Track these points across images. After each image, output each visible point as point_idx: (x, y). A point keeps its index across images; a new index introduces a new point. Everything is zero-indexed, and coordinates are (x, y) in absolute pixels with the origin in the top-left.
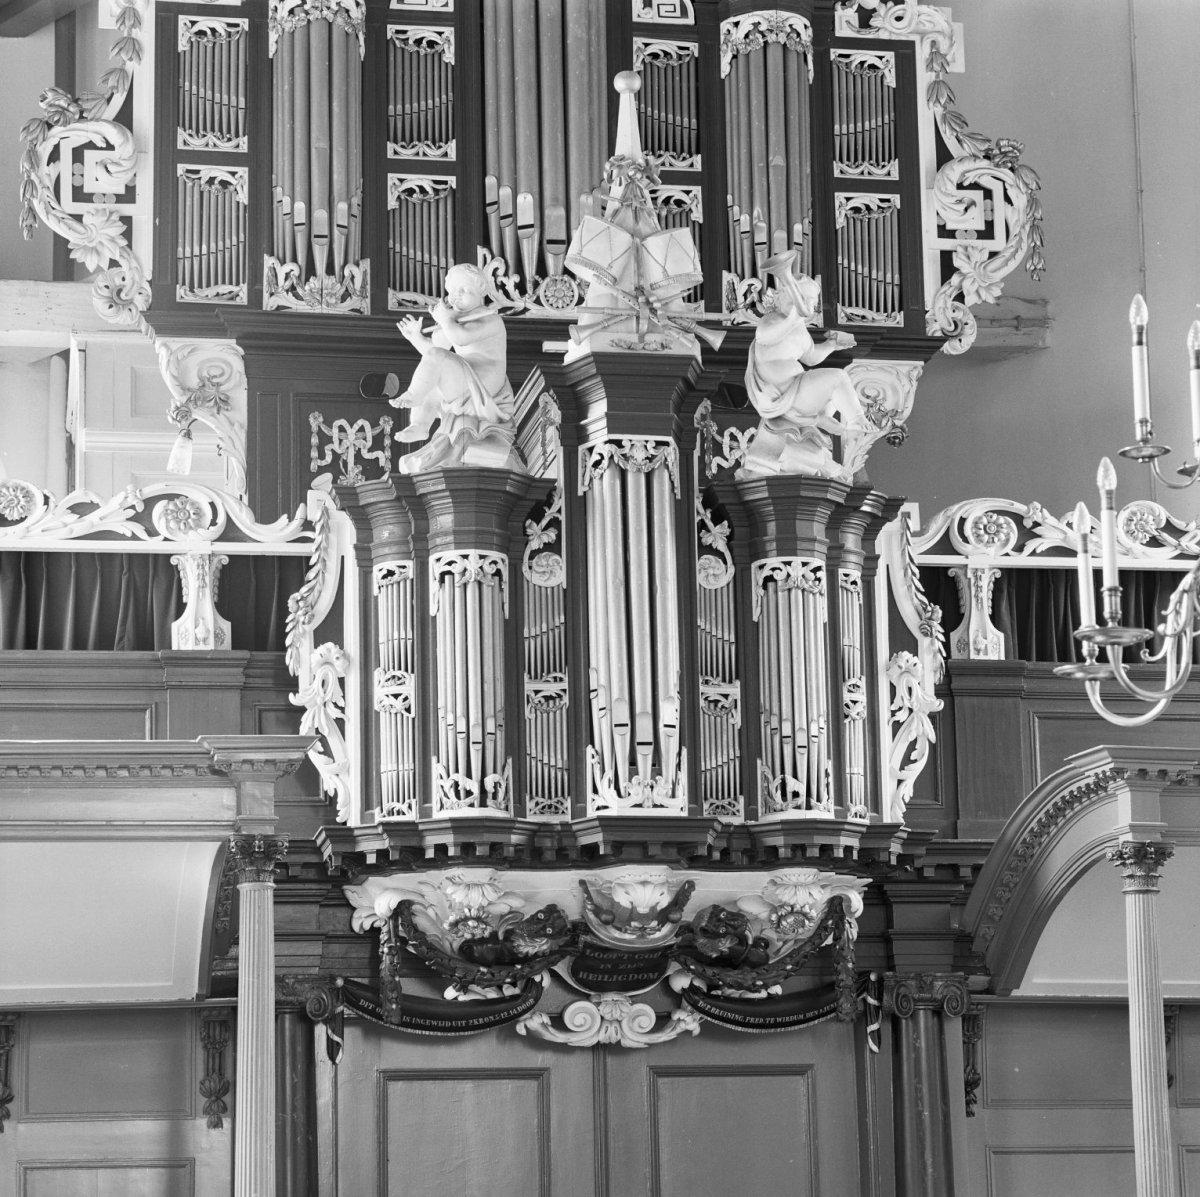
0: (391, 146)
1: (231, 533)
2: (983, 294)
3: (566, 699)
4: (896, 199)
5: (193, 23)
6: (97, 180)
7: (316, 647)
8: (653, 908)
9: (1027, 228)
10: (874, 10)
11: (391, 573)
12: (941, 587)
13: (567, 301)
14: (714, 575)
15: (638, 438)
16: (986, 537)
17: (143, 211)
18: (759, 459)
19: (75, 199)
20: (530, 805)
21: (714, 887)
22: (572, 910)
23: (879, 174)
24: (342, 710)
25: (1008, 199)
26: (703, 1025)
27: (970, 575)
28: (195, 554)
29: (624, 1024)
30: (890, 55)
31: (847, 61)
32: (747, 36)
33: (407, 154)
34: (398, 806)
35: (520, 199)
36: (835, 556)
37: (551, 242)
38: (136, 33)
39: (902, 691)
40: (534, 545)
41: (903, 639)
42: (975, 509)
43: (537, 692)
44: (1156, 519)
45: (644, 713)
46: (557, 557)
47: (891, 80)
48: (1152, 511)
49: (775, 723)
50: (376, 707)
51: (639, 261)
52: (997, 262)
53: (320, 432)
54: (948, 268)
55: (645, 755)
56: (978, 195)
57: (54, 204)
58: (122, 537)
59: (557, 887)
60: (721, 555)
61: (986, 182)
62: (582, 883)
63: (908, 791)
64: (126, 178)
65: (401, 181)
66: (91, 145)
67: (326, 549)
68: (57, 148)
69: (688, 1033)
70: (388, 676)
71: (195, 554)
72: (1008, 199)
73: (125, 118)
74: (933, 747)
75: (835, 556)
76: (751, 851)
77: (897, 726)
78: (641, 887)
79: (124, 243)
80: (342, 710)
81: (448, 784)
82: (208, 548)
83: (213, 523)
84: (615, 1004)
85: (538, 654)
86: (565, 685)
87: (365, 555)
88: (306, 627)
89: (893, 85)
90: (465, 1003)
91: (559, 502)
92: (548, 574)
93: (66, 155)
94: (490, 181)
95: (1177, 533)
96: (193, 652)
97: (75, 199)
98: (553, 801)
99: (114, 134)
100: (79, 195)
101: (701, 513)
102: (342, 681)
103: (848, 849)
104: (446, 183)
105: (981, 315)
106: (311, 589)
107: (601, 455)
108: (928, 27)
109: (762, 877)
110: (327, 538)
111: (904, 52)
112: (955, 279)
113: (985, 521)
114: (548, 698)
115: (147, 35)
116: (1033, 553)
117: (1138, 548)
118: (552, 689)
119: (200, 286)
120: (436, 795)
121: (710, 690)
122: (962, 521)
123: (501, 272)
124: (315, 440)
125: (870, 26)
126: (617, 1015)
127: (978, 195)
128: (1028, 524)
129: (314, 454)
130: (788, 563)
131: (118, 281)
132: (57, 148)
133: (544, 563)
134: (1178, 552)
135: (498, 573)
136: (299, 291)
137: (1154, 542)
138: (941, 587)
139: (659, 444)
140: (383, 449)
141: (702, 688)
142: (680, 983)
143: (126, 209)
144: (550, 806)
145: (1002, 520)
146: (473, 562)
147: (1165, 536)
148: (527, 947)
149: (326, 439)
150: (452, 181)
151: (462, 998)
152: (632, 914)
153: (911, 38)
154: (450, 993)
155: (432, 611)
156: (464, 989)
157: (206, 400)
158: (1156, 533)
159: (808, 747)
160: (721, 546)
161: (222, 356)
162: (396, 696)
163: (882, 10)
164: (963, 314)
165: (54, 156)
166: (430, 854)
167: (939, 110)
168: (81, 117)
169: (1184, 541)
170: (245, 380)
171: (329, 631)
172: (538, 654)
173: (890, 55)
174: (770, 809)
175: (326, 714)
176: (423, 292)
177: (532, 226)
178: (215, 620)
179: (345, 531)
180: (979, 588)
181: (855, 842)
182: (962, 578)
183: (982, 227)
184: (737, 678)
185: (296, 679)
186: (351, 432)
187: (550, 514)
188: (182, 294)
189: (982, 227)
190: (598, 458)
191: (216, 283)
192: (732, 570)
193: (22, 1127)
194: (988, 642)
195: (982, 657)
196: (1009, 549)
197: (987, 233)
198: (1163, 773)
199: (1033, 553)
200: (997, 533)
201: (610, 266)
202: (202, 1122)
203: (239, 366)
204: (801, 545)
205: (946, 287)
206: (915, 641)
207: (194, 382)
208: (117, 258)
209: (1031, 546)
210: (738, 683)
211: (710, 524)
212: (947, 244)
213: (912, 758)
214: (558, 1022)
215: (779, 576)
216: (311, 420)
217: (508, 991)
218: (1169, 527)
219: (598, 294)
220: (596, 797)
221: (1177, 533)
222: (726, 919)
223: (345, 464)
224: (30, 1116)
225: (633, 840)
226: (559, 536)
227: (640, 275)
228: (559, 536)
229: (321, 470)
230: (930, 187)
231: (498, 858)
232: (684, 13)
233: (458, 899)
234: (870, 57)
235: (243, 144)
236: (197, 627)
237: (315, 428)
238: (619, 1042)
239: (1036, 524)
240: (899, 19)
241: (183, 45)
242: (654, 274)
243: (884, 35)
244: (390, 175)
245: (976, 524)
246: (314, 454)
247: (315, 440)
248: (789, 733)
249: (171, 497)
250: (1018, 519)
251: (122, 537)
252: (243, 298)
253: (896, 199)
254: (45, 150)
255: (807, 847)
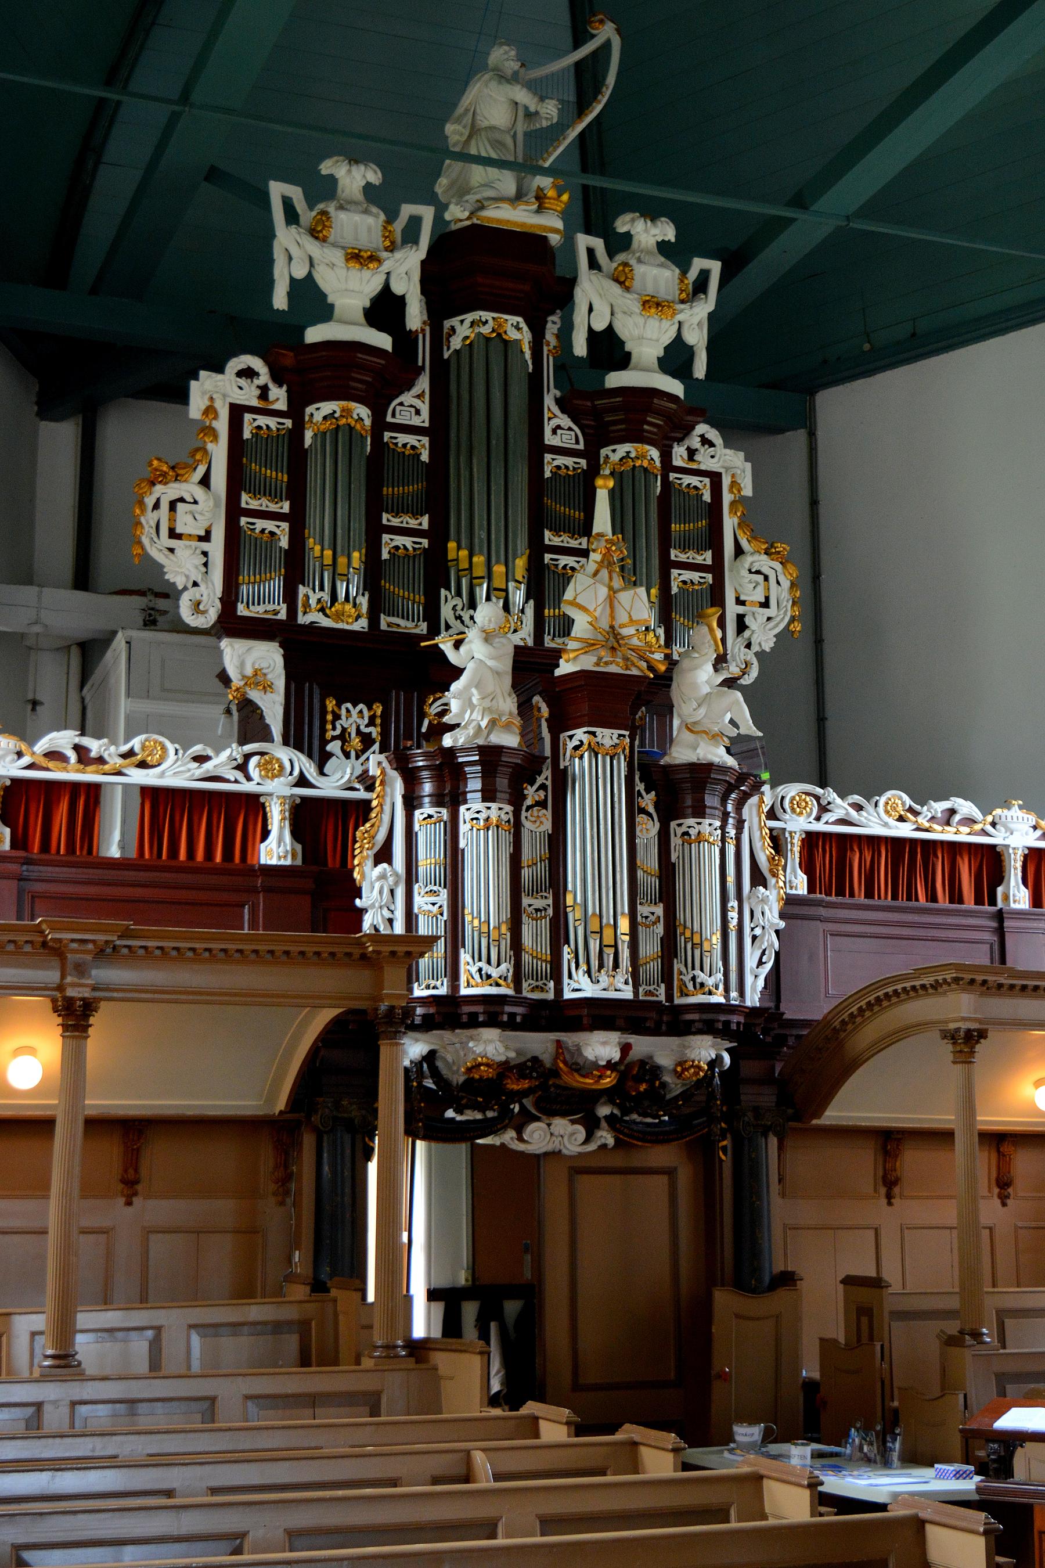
0: (385, 516)
1: (302, 781)
2: (763, 644)
3: (550, 911)
4: (709, 577)
5: (254, 420)
6: (185, 523)
7: (376, 865)
8: (609, 1062)
9: (791, 602)
10: (697, 450)
11: (430, 816)
12: (777, 841)
13: (506, 630)
14: (648, 830)
15: (607, 732)
16: (798, 810)
17: (217, 548)
18: (684, 751)
19: (170, 537)
20: (525, 985)
21: (643, 1045)
22: (547, 1059)
23: (699, 559)
24: (392, 912)
25: (778, 583)
26: (617, 1140)
27: (787, 835)
28: (277, 794)
29: (566, 1138)
30: (707, 481)
31: (679, 482)
32: (621, 460)
33: (395, 522)
34: (433, 983)
35: (475, 559)
36: (725, 816)
37: (496, 589)
38: (215, 424)
39: (758, 914)
40: (529, 802)
41: (758, 879)
42: (792, 790)
43: (530, 906)
44: (904, 804)
45: (608, 924)
46: (544, 811)
47: (707, 497)
48: (900, 798)
49: (688, 934)
50: (416, 910)
51: (612, 607)
52: (772, 624)
53: (333, 712)
54: (741, 626)
55: (610, 961)
56: (760, 578)
57: (156, 539)
58: (228, 781)
59: (539, 1043)
60: (650, 815)
61: (765, 570)
62: (558, 1042)
63: (761, 983)
64: (206, 525)
65: (392, 540)
66: (182, 500)
67: (383, 797)
68: (158, 500)
69: (604, 1146)
70: (428, 889)
71: (277, 794)
72: (778, 583)
73: (205, 482)
74: (777, 954)
75: (725, 816)
76: (676, 1021)
77: (754, 938)
78: (601, 1047)
79: (204, 569)
80: (392, 912)
81: (474, 970)
82: (289, 791)
83: (291, 774)
84: (561, 1125)
85: (539, 877)
86: (550, 901)
87: (411, 803)
88: (370, 852)
89: (709, 501)
90: (461, 1122)
91: (547, 773)
92: (538, 824)
93: (165, 506)
94: (452, 545)
95: (916, 813)
96: (276, 866)
97: (170, 537)
98: (540, 983)
99: (199, 493)
100: (173, 534)
101: (640, 787)
102: (392, 891)
103: (738, 1023)
104: (420, 543)
105: (760, 655)
106: (372, 826)
107: (581, 741)
108: (732, 465)
109: (673, 1041)
110: (383, 790)
111: (715, 478)
112: (747, 634)
113: (797, 798)
114: (537, 910)
115: (222, 426)
116: (827, 823)
117: (891, 822)
118: (539, 903)
119: (253, 604)
120: (463, 978)
121: (643, 910)
122: (783, 798)
123: (459, 608)
124: (330, 717)
125: (694, 461)
126: (562, 1133)
127: (760, 578)
128: (824, 802)
129: (329, 727)
130: (700, 823)
131: (198, 597)
132: (158, 500)
133: (535, 814)
134: (915, 827)
135: (509, 821)
136: (328, 611)
137: (901, 819)
138: (777, 841)
139: (620, 735)
140: (375, 725)
141: (639, 907)
142: (604, 1111)
143: (205, 546)
144: (537, 987)
145: (808, 799)
146: (498, 811)
147: (909, 815)
148: (513, 1085)
149: (337, 717)
150: (425, 542)
151: (459, 1118)
152: (595, 1065)
153: (722, 470)
154: (450, 1113)
155: (462, 844)
156: (459, 1111)
157: (257, 684)
158: (902, 813)
159: (616, 946)
160: (651, 809)
161: (268, 657)
162: (434, 904)
163: (702, 450)
164: (750, 656)
165: (156, 506)
166: (465, 1018)
167: (736, 520)
168: (176, 480)
169: (920, 819)
170: (284, 672)
171: (384, 855)
172: (539, 877)
173: (707, 481)
174: (684, 994)
175: (382, 915)
176: (403, 618)
177: (483, 578)
178: (292, 845)
179: (398, 787)
180: (792, 844)
181: (742, 1019)
182: (781, 837)
183: (763, 600)
184: (660, 901)
185: (360, 889)
186: (354, 712)
187: (540, 780)
188: (242, 610)
189: (763, 600)
190: (578, 743)
191: (259, 604)
192: (657, 825)
193: (152, 1203)
194: (800, 885)
195: (794, 892)
196: (811, 819)
197: (766, 604)
198: (985, 982)
199: (827, 823)
200: (805, 808)
201: (595, 610)
202: (272, 1200)
203: (280, 661)
204: (708, 811)
205: (740, 639)
206: (765, 879)
207: (249, 671)
208: (199, 581)
209: (826, 817)
210: (661, 905)
211: (644, 793)
212: (741, 610)
213: (764, 960)
214: (520, 1139)
215: (693, 832)
216: (328, 702)
217: (490, 1114)
218: (911, 810)
219: (581, 626)
220: (571, 982)
221: (916, 813)
222: (648, 1070)
223: (350, 734)
224: (148, 1197)
225: (600, 1014)
226: (546, 796)
227: (612, 617)
228: (546, 796)
229: (334, 738)
230: (731, 570)
231: (511, 1025)
232: (577, 442)
233: (490, 1045)
234: (694, 481)
235: (286, 507)
236: (276, 849)
237: (330, 709)
238: (560, 1151)
239: (829, 803)
240: (712, 457)
241: (247, 435)
242: (622, 617)
243: (703, 467)
244: (384, 535)
245: (791, 802)
246: (329, 727)
247: (330, 717)
248: (699, 942)
249: (262, 754)
250: (818, 798)
251: (228, 781)
252: (283, 615)
253: (709, 577)
254: (150, 501)
255: (710, 1020)
